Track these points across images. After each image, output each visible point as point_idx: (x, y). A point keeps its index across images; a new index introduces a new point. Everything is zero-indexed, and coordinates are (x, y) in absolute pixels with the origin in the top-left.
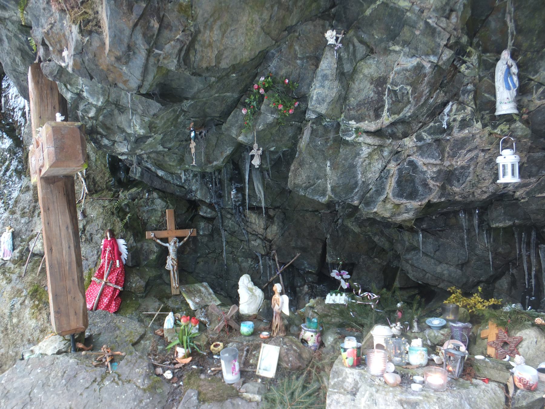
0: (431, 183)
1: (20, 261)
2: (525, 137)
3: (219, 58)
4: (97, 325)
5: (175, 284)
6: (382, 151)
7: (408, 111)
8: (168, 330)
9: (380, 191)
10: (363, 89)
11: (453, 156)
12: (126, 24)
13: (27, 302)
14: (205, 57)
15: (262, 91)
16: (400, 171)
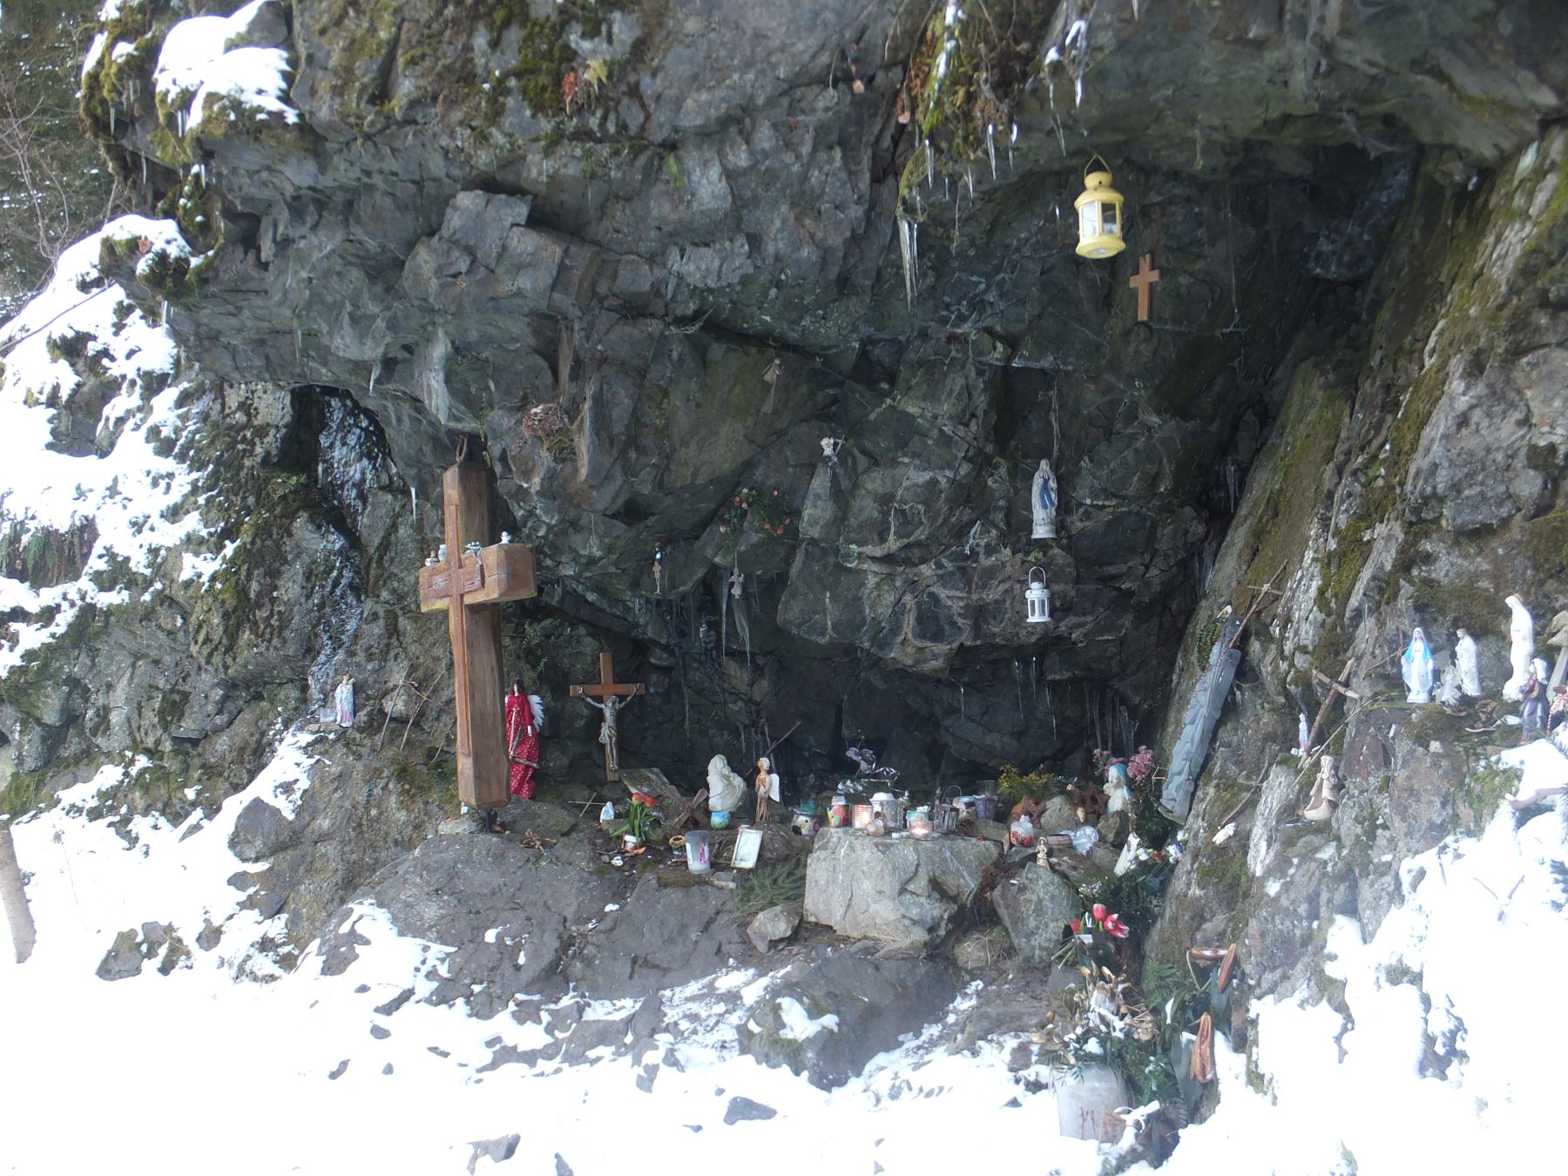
0: (960, 621)
1: (370, 728)
2: (1069, 565)
3: (694, 475)
4: (509, 813)
5: (612, 764)
6: (893, 581)
7: (921, 534)
8: (608, 822)
9: (896, 629)
10: (865, 508)
11: (984, 587)
12: (607, 461)
13: (391, 786)
14: (681, 475)
15: (744, 505)
16: (919, 605)
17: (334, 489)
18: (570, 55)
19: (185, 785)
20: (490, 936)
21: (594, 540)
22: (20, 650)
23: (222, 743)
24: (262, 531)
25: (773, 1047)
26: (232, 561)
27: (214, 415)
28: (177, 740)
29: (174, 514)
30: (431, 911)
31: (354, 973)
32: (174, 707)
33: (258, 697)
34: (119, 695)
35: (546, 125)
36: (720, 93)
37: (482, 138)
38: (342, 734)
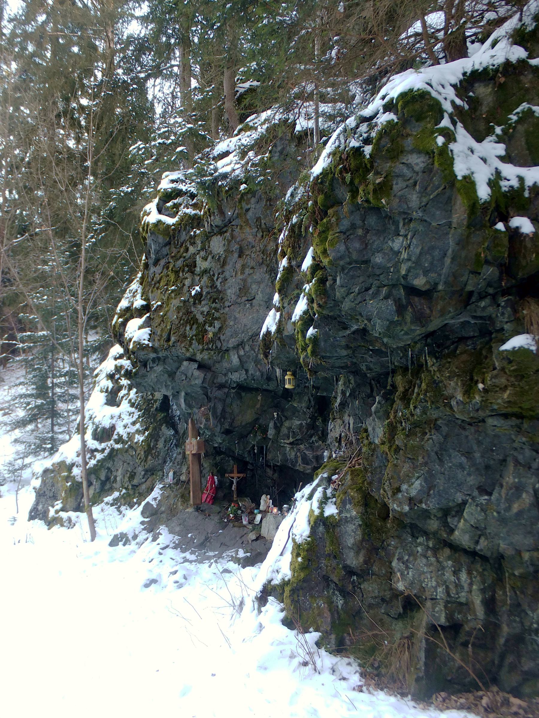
1: (177, 484)
4: (204, 506)
7: (298, 437)
9: (297, 462)
10: (284, 430)
14: (237, 423)
18: (206, 331)
19: (134, 498)
20: (189, 535)
22: (96, 460)
23: (144, 487)
24: (155, 429)
25: (237, 560)
26: (147, 437)
27: (145, 396)
28: (133, 485)
29: (134, 423)
30: (177, 529)
31: (158, 541)
32: (132, 476)
33: (153, 474)
34: (119, 473)
36: (237, 339)
37: (188, 350)
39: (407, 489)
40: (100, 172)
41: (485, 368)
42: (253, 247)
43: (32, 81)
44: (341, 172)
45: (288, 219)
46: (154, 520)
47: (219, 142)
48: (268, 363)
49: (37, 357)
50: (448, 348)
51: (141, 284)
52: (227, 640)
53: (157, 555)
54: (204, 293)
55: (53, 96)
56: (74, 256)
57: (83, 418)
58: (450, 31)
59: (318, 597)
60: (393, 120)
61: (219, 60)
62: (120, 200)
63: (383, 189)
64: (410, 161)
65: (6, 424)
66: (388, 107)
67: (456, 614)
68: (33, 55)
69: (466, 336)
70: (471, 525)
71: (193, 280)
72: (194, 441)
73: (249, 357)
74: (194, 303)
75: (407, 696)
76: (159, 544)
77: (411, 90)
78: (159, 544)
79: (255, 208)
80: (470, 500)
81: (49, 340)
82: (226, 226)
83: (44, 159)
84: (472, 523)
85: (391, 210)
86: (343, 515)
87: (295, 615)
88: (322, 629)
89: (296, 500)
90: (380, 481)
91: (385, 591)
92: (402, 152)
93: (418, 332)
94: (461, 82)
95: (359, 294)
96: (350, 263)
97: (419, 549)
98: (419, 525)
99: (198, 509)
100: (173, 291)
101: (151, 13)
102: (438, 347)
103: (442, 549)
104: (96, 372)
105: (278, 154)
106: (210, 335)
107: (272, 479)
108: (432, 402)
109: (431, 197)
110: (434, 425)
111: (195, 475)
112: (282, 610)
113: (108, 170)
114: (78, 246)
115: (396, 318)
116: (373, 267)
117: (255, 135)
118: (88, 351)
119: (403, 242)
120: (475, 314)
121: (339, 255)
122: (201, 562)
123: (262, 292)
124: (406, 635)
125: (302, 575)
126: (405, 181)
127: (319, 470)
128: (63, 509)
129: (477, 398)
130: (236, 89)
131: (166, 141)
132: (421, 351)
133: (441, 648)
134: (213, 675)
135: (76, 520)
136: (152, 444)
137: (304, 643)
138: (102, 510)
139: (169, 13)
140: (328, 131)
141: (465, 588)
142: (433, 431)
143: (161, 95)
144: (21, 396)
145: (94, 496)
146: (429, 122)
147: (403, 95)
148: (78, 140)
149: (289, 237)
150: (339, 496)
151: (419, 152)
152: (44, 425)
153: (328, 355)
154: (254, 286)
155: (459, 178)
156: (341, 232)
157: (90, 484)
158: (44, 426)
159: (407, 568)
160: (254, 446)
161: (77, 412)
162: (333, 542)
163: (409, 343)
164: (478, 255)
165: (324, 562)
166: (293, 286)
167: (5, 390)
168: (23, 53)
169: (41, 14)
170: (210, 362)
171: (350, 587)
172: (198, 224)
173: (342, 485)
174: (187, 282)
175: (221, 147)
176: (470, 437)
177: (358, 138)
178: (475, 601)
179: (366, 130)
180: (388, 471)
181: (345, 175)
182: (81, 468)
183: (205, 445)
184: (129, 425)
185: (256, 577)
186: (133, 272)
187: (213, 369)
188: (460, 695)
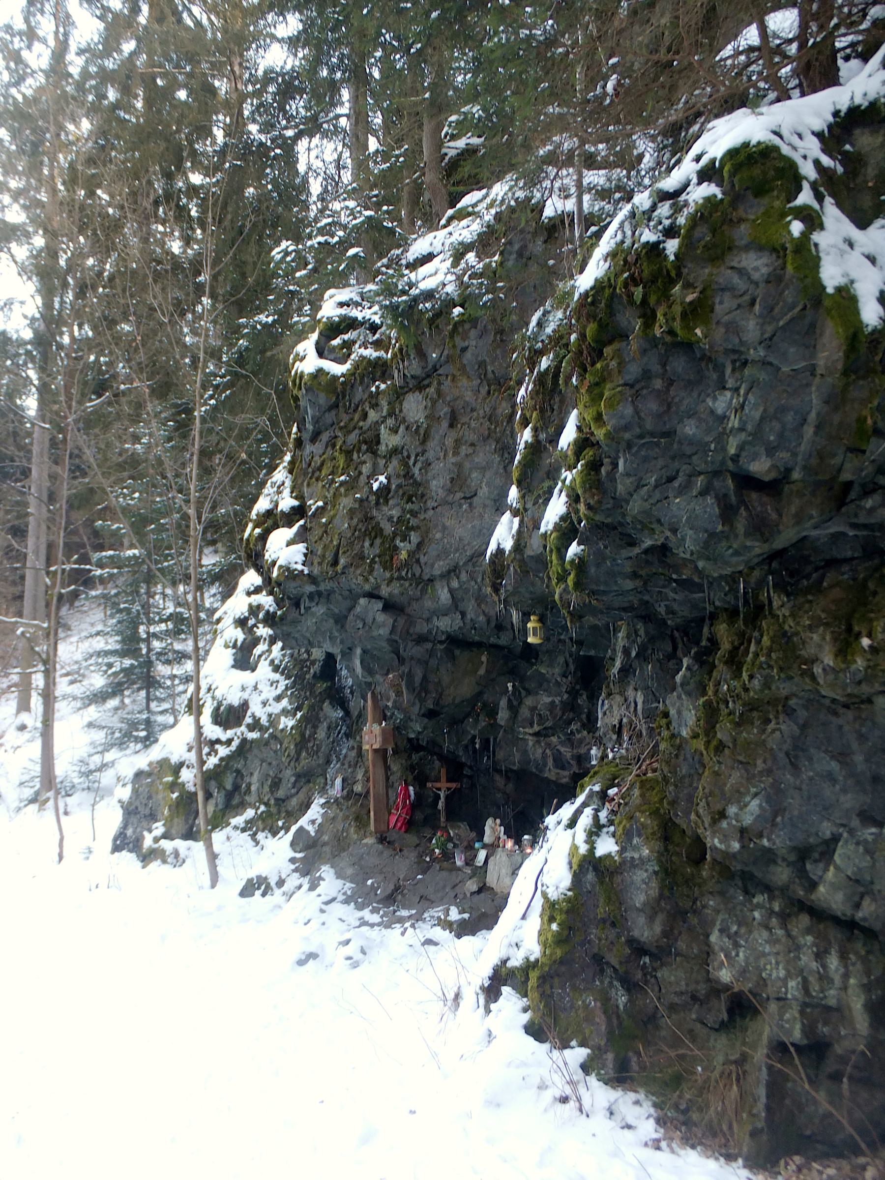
1: (347, 797)
4: (393, 836)
7: (549, 724)
9: (545, 765)
10: (525, 712)
12: (412, 698)
14: (447, 700)
17: (342, 689)
18: (396, 548)
19: (278, 820)
20: (369, 882)
21: (418, 725)
22: (218, 757)
23: (294, 802)
24: (312, 708)
25: (447, 925)
26: (299, 721)
27: (296, 654)
28: (276, 800)
29: (278, 699)
30: (350, 871)
31: (319, 890)
32: (276, 784)
33: (309, 781)
34: (255, 778)
35: (388, 575)
36: (447, 562)
37: (367, 580)
38: (336, 800)
39: (736, 814)
40: (221, 291)
41: (872, 611)
42: (473, 410)
43: (113, 147)
44: (626, 285)
45: (533, 362)
46: (311, 855)
47: (415, 240)
48: (500, 601)
49: (124, 591)
50: (808, 577)
51: (291, 472)
52: (434, 1055)
53: (319, 912)
54: (394, 487)
55: (147, 171)
56: (183, 428)
57: (198, 688)
58: (811, 42)
59: (586, 989)
60: (715, 196)
61: (415, 104)
62: (254, 336)
63: (698, 312)
64: (744, 264)
65: (75, 698)
66: (706, 175)
67: (820, 1026)
68: (116, 106)
69: (839, 556)
70: (848, 876)
71: (375, 465)
72: (376, 729)
73: (467, 591)
74: (377, 503)
75: (736, 1160)
76: (319, 895)
77: (746, 145)
78: (319, 895)
79: (475, 346)
80: (845, 835)
81: (144, 562)
82: (428, 376)
83: (134, 272)
84: (849, 873)
85: (711, 347)
86: (628, 855)
87: (547, 1019)
88: (591, 1043)
89: (547, 828)
90: (690, 799)
91: (697, 983)
92: (730, 249)
93: (757, 551)
94: (830, 127)
95: (656, 487)
96: (641, 437)
97: (757, 914)
98: (756, 874)
99: (382, 840)
100: (342, 483)
101: (305, 30)
102: (791, 575)
103: (797, 916)
104: (217, 616)
105: (514, 256)
106: (403, 555)
107: (504, 793)
108: (781, 669)
109: (781, 323)
110: (784, 706)
111: (377, 786)
112: (525, 1010)
113: (235, 289)
114: (189, 411)
115: (720, 528)
116: (679, 442)
117: (476, 227)
118: (203, 580)
119: (731, 400)
120: (855, 521)
121: (623, 422)
122: (388, 926)
123: (488, 484)
124: (733, 1058)
125: (559, 953)
126: (735, 297)
127: (587, 779)
128: (166, 836)
129: (860, 663)
130: (444, 151)
131: (330, 240)
132: (762, 582)
133: (795, 1081)
134: (413, 1112)
135: (187, 853)
136: (308, 732)
137: (562, 1065)
138: (228, 838)
139: (333, 30)
140: (600, 217)
141: (836, 982)
142: (782, 717)
143: (321, 164)
144: (99, 654)
145: (215, 816)
146: (778, 197)
147: (732, 154)
148: (187, 241)
149: (534, 394)
150: (620, 823)
151: (760, 248)
152: (134, 700)
153: (602, 588)
154: (474, 475)
155: (830, 290)
156: (625, 385)
157: (208, 796)
158: (134, 701)
159: (736, 945)
160: (474, 737)
161: (187, 679)
162: (610, 899)
163: (741, 568)
164: (861, 420)
165: (594, 933)
166: (542, 474)
167: (72, 643)
168: (101, 103)
169: (127, 40)
170: (404, 599)
171: (639, 975)
172: (384, 373)
173: (626, 804)
174: (366, 469)
175: (419, 247)
176: (846, 728)
177: (655, 227)
178: (852, 1005)
179: (668, 214)
180: (705, 783)
181: (633, 289)
182: (195, 771)
183: (394, 736)
184: (271, 701)
185: (484, 952)
186: (276, 454)
187: (408, 610)
188: (828, 1163)
